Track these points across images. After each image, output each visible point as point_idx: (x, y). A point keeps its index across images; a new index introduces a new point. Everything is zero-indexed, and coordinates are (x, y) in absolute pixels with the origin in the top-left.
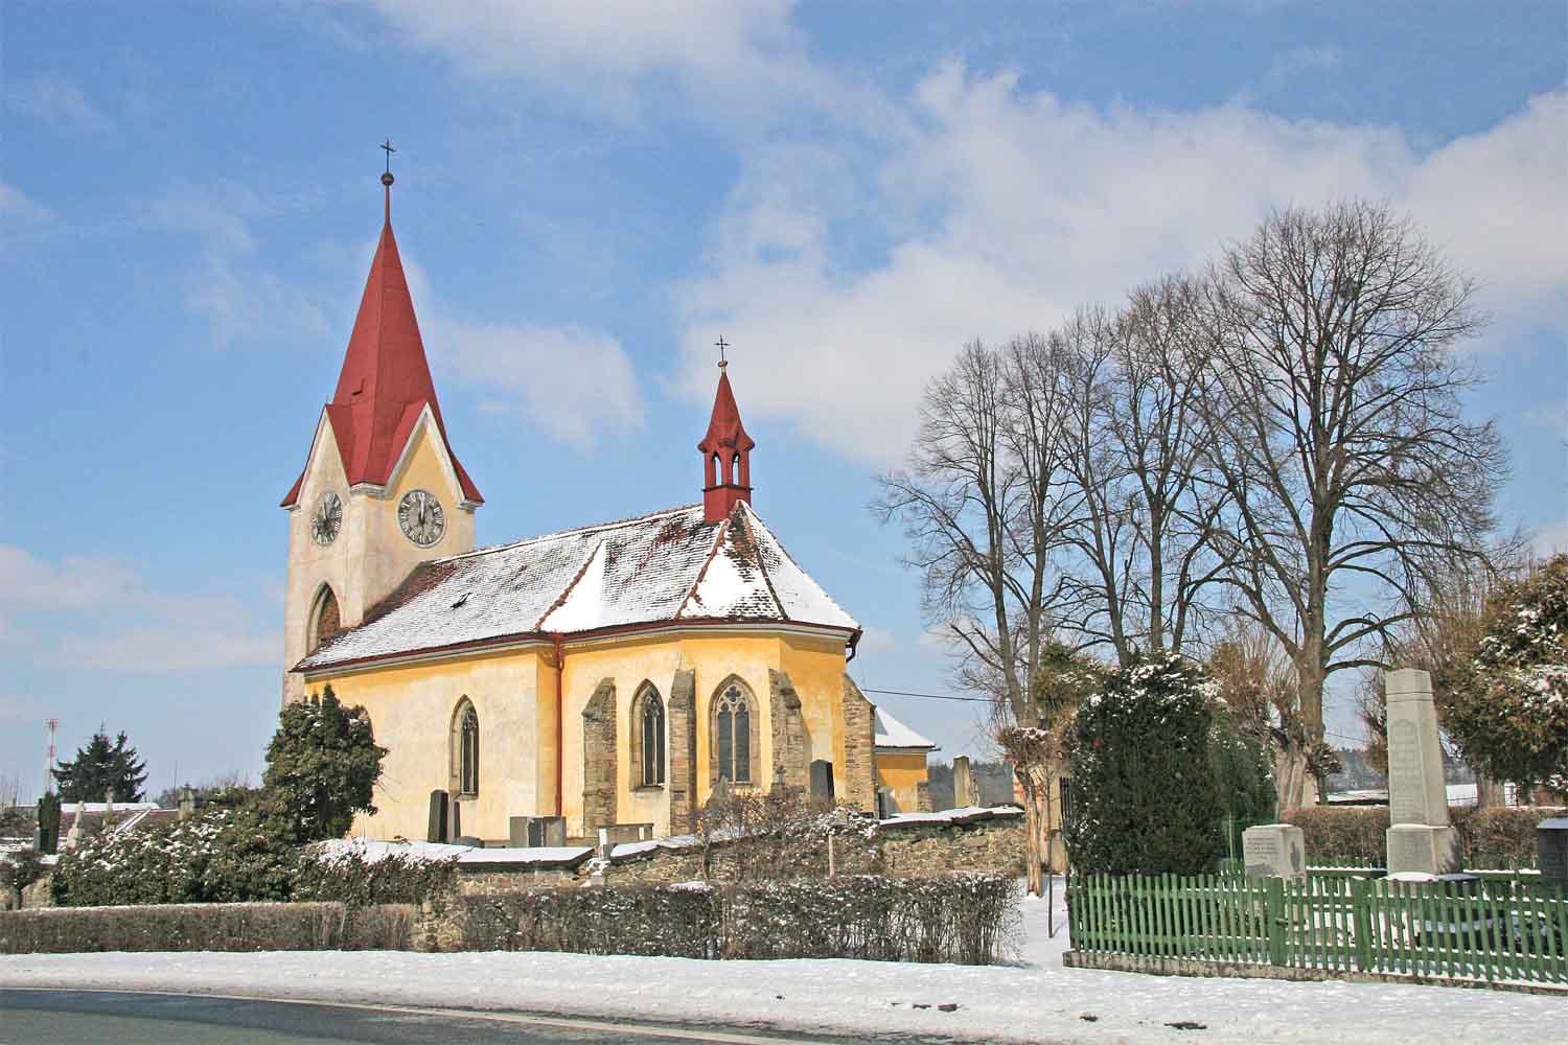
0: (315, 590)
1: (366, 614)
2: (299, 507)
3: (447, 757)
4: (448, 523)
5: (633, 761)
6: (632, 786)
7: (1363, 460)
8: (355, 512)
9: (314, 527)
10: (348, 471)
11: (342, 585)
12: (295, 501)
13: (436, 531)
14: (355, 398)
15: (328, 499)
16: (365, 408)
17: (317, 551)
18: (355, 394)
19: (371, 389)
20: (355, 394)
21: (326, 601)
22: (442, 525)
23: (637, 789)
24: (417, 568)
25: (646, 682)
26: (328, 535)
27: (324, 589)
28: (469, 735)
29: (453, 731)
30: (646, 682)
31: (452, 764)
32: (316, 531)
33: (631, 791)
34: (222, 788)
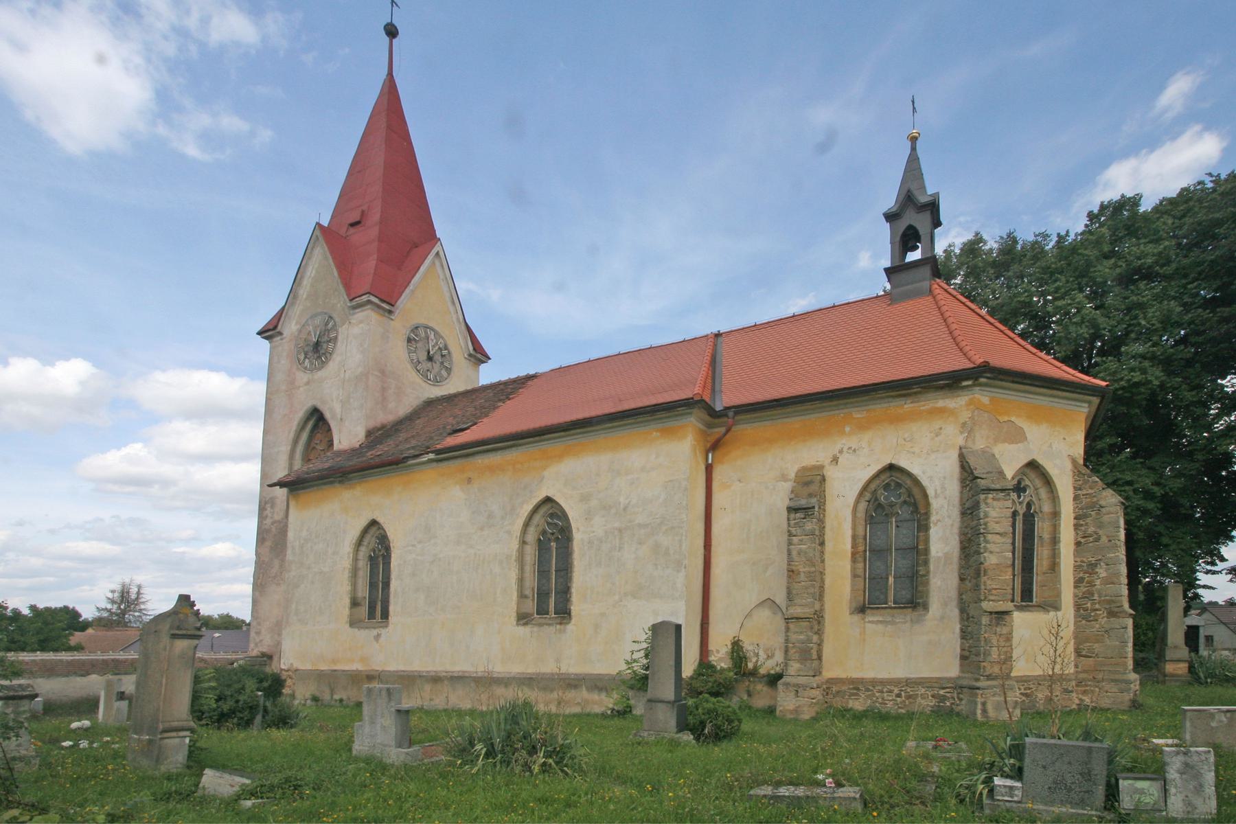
0: (300, 415)
1: (369, 433)
2: (280, 333)
3: (513, 575)
4: (455, 370)
5: (855, 576)
6: (854, 605)
7: (1100, 372)
8: (356, 330)
9: (299, 353)
10: (347, 286)
11: (337, 407)
12: (276, 327)
13: (444, 373)
14: (352, 230)
15: (318, 321)
16: (367, 237)
17: (302, 377)
18: (353, 225)
19: (375, 217)
20: (353, 225)
21: (315, 427)
22: (450, 369)
23: (862, 610)
24: (425, 402)
25: (374, 523)
26: (319, 357)
27: (365, 531)
28: (549, 549)
29: (523, 542)
30: (374, 523)
31: (521, 580)
32: (302, 357)
33: (851, 614)
34: (1207, 179)
